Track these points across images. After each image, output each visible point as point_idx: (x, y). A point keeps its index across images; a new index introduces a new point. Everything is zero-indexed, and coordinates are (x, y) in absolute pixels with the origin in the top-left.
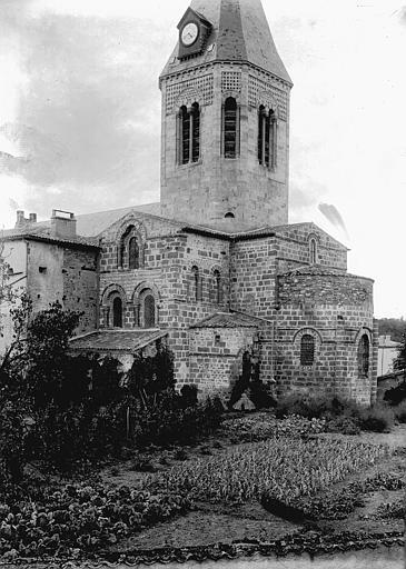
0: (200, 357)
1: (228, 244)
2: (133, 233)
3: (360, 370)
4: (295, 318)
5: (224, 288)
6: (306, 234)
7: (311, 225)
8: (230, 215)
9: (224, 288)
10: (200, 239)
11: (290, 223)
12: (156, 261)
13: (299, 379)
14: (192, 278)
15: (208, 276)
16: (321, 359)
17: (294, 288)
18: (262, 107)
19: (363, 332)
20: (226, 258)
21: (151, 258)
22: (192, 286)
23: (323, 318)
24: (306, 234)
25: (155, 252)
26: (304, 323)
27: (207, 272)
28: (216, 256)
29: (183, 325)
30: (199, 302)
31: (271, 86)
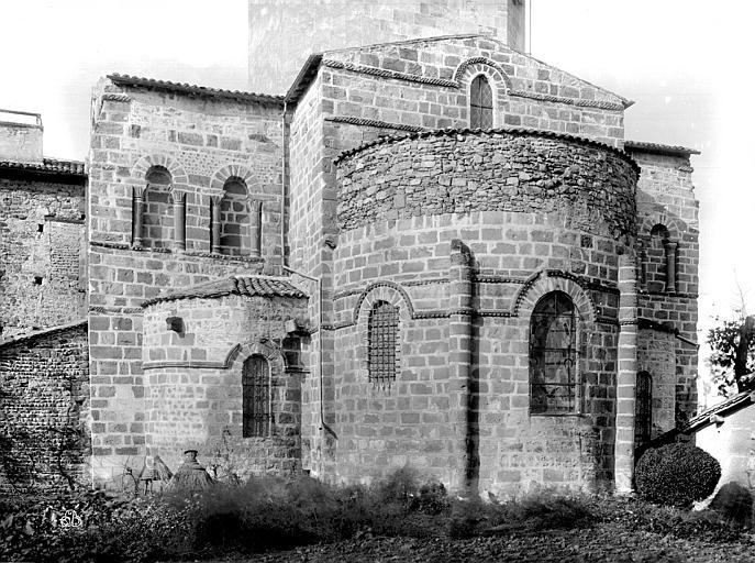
4: (360, 262)
16: (413, 362)
23: (415, 254)
27: (203, 181)
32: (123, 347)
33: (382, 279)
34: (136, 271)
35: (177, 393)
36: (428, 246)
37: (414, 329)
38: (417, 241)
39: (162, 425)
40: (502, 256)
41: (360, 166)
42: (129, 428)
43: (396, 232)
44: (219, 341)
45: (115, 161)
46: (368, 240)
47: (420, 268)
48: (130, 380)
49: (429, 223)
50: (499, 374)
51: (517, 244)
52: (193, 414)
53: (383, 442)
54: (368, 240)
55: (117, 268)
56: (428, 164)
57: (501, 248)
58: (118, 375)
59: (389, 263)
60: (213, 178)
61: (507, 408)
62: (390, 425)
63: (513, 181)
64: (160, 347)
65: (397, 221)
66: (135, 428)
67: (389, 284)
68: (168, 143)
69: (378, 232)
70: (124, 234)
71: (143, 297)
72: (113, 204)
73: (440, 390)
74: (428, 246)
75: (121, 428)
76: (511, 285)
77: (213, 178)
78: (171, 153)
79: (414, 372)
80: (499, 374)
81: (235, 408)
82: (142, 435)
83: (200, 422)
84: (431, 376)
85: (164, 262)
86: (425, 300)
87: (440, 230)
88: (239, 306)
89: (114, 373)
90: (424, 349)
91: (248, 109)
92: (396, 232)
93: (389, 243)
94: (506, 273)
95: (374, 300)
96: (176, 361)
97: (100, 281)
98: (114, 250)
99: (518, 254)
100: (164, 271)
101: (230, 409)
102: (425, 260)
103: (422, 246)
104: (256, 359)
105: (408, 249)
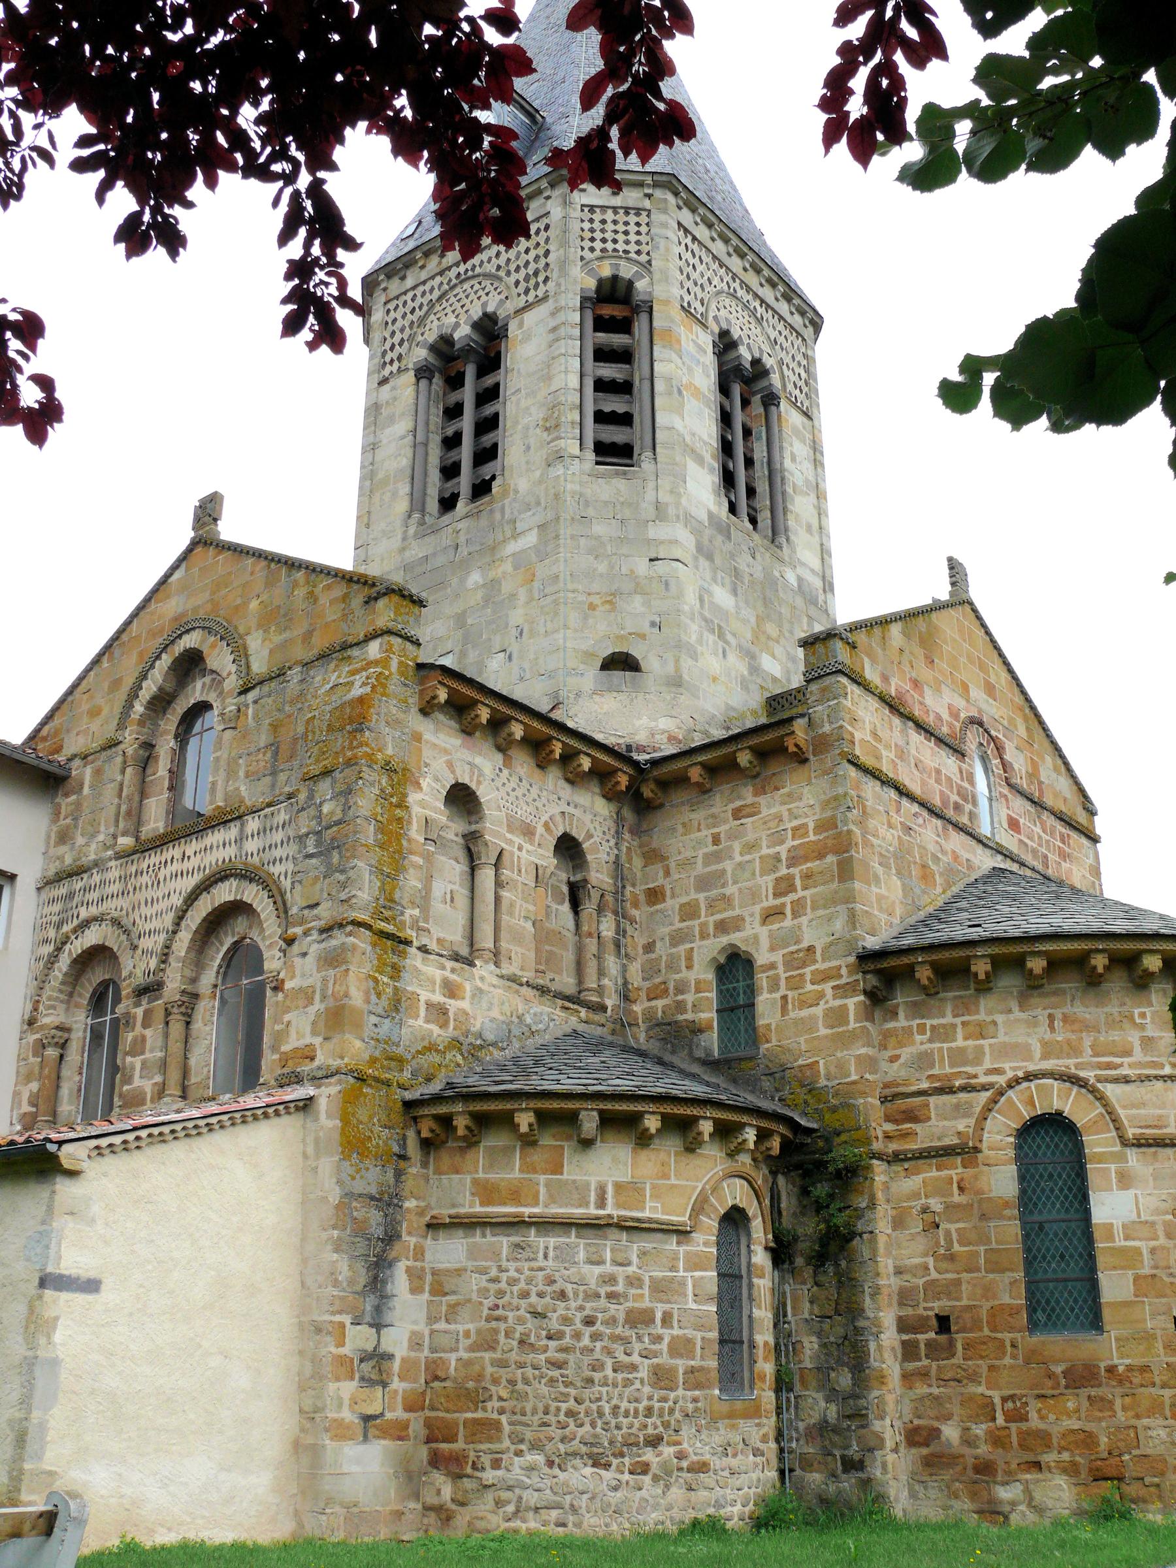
8: (621, 663)
33: (1048, 1065)
60: (540, 830)
77: (540, 830)
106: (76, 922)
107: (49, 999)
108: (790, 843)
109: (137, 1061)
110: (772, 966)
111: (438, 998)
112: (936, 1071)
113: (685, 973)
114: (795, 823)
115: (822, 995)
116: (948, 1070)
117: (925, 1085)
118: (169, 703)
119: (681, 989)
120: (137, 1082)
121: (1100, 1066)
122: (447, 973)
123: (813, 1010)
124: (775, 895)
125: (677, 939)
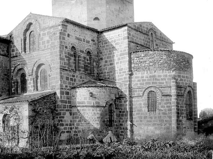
0: (84, 82)
1: (95, 35)
2: (32, 28)
3: (187, 115)
4: (143, 80)
5: (95, 64)
6: (147, 28)
7: (150, 24)
8: (96, 19)
9: (95, 64)
10: (76, 28)
11: (135, 21)
12: (46, 45)
13: (148, 121)
14: (71, 55)
15: (83, 55)
16: (162, 107)
17: (141, 60)
18: (117, 50)
19: (188, 89)
20: (95, 44)
21: (43, 43)
22: (72, 60)
23: (162, 79)
24: (147, 28)
25: (46, 38)
26: (150, 83)
27: (82, 52)
28: (88, 42)
29: (66, 86)
30: (77, 72)
31: (14, 61)
32: (67, 100)
33: (152, 85)
34: (70, 77)
35: (90, 114)
36: (165, 78)
37: (162, 98)
38: (162, 77)
39: (84, 124)
40: (181, 82)
41: (142, 55)
42: (69, 125)
43: (156, 74)
44: (103, 100)
45: (64, 44)
46: (147, 75)
47: (163, 83)
48: (69, 110)
49: (165, 72)
50: (181, 110)
51: (183, 79)
52: (96, 120)
53: (153, 127)
54: (147, 75)
55: (66, 76)
56: (165, 58)
57: (181, 80)
58: (66, 109)
59: (154, 81)
60: (85, 51)
61: (183, 118)
62: (155, 123)
63: (182, 64)
64: (83, 100)
65: (156, 71)
66: (70, 125)
67: (155, 87)
68: (75, 40)
69: (151, 73)
70: (67, 66)
71: (71, 85)
72: (64, 57)
73: (169, 114)
74: (165, 78)
75: (67, 125)
76: (183, 89)
77: (85, 51)
78: (76, 43)
79: (162, 109)
80: (181, 110)
81: (107, 119)
82: (71, 127)
83: (98, 123)
84: (167, 111)
85: (75, 75)
86: (165, 91)
87: (168, 74)
88: (107, 90)
89: (65, 108)
90: (165, 104)
91: (92, 32)
92: (156, 74)
93: (154, 76)
94: (182, 86)
95: (149, 90)
96: (91, 105)
97: (62, 80)
98: (65, 71)
99: (184, 82)
100: (75, 78)
101: (106, 119)
102: (164, 81)
103: (164, 78)
104: (111, 105)
105: (160, 78)
106: (17, 65)
107: (15, 76)
108: (120, 53)
109: (30, 85)
110: (117, 70)
111: (72, 77)
112: (138, 86)
113: (106, 71)
114: (121, 50)
115: (123, 75)
116: (139, 86)
117: (136, 87)
118: (27, 30)
119: (105, 73)
120: (30, 88)
121: (160, 85)
122: (73, 74)
123: (122, 77)
124: (118, 60)
125: (105, 65)
